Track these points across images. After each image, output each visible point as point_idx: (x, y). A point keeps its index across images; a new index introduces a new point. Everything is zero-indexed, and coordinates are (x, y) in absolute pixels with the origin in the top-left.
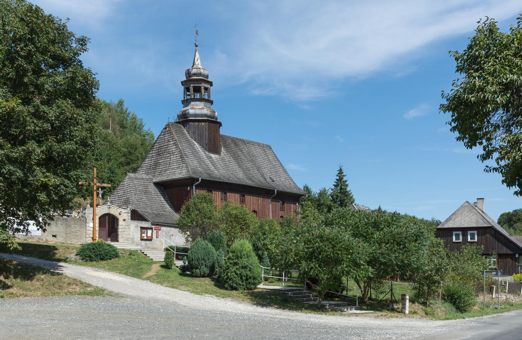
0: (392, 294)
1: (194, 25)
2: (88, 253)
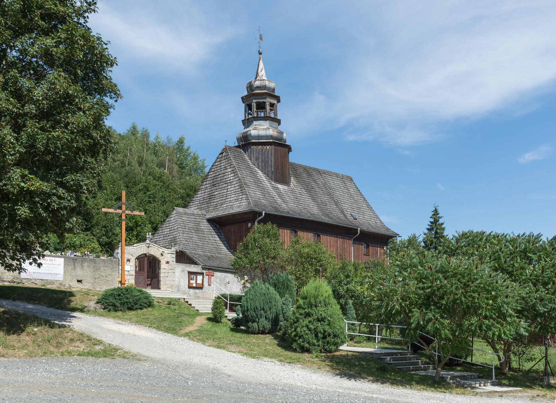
0: (547, 363)
1: (258, 29)
2: (112, 300)
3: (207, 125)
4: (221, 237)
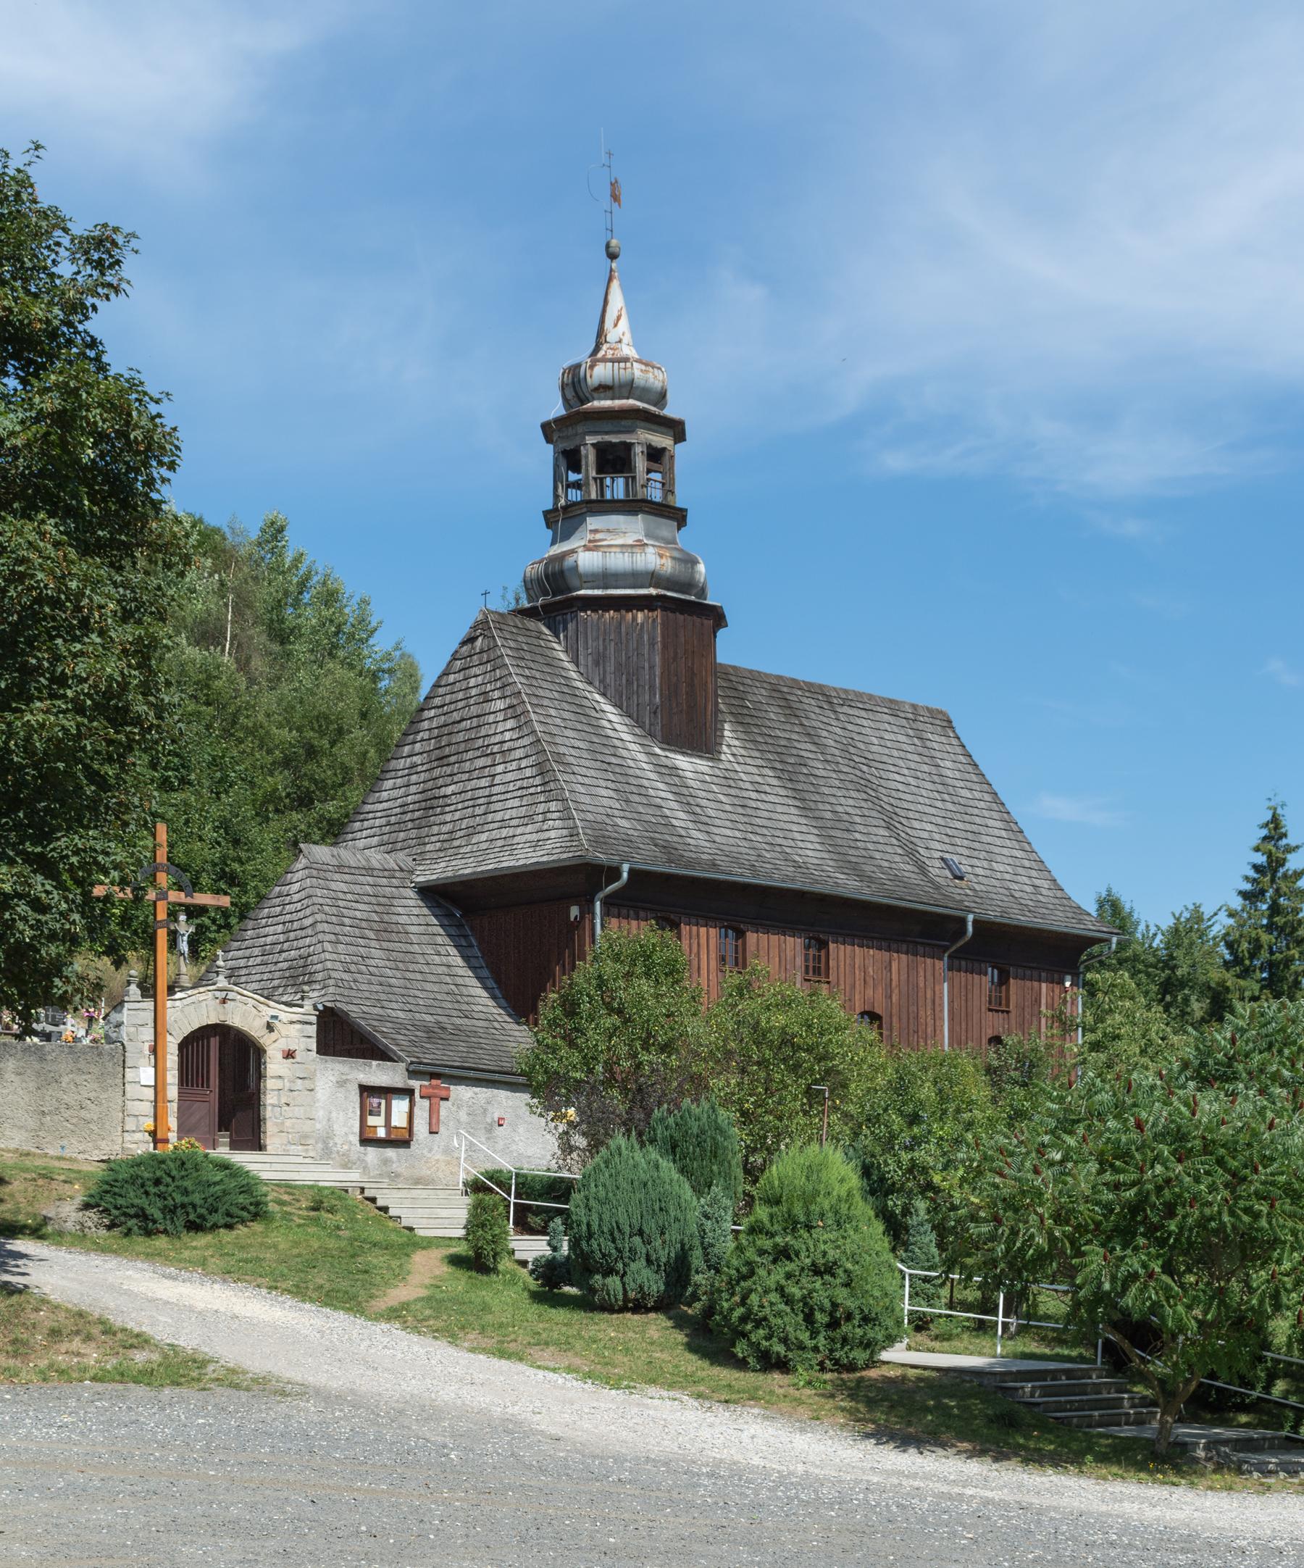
2: (134, 1197)
4: (469, 952)
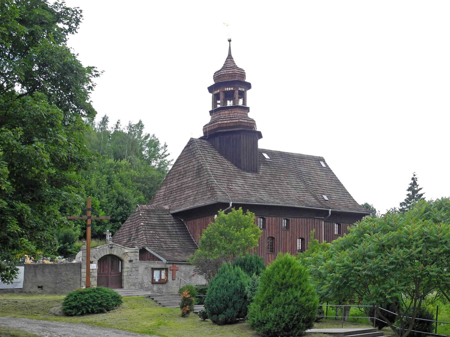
3: (175, 122)
